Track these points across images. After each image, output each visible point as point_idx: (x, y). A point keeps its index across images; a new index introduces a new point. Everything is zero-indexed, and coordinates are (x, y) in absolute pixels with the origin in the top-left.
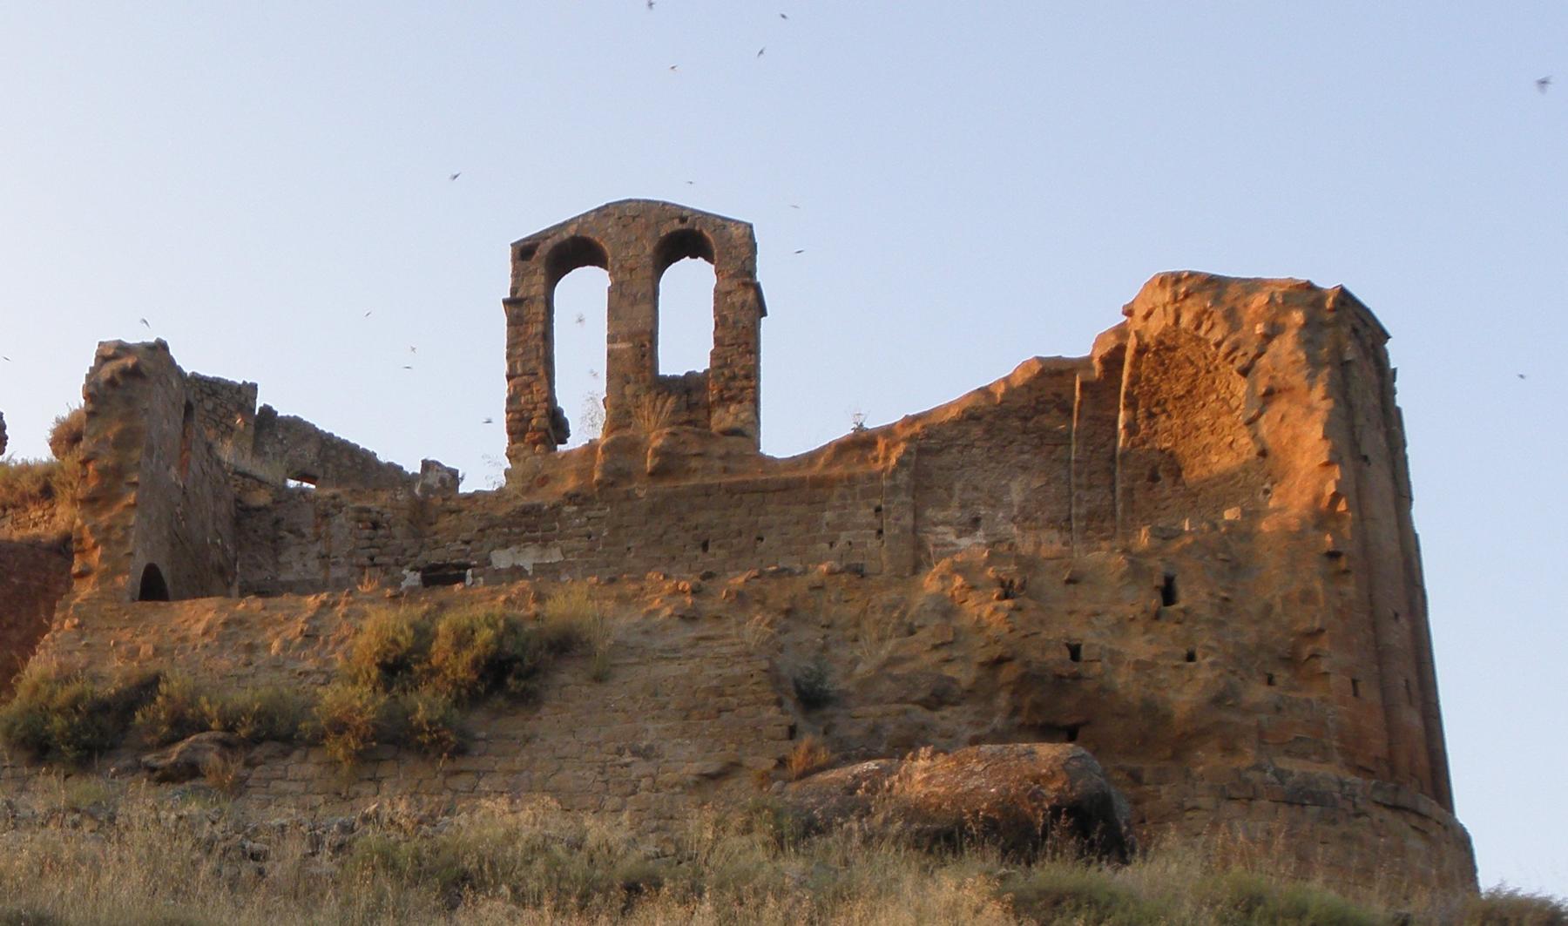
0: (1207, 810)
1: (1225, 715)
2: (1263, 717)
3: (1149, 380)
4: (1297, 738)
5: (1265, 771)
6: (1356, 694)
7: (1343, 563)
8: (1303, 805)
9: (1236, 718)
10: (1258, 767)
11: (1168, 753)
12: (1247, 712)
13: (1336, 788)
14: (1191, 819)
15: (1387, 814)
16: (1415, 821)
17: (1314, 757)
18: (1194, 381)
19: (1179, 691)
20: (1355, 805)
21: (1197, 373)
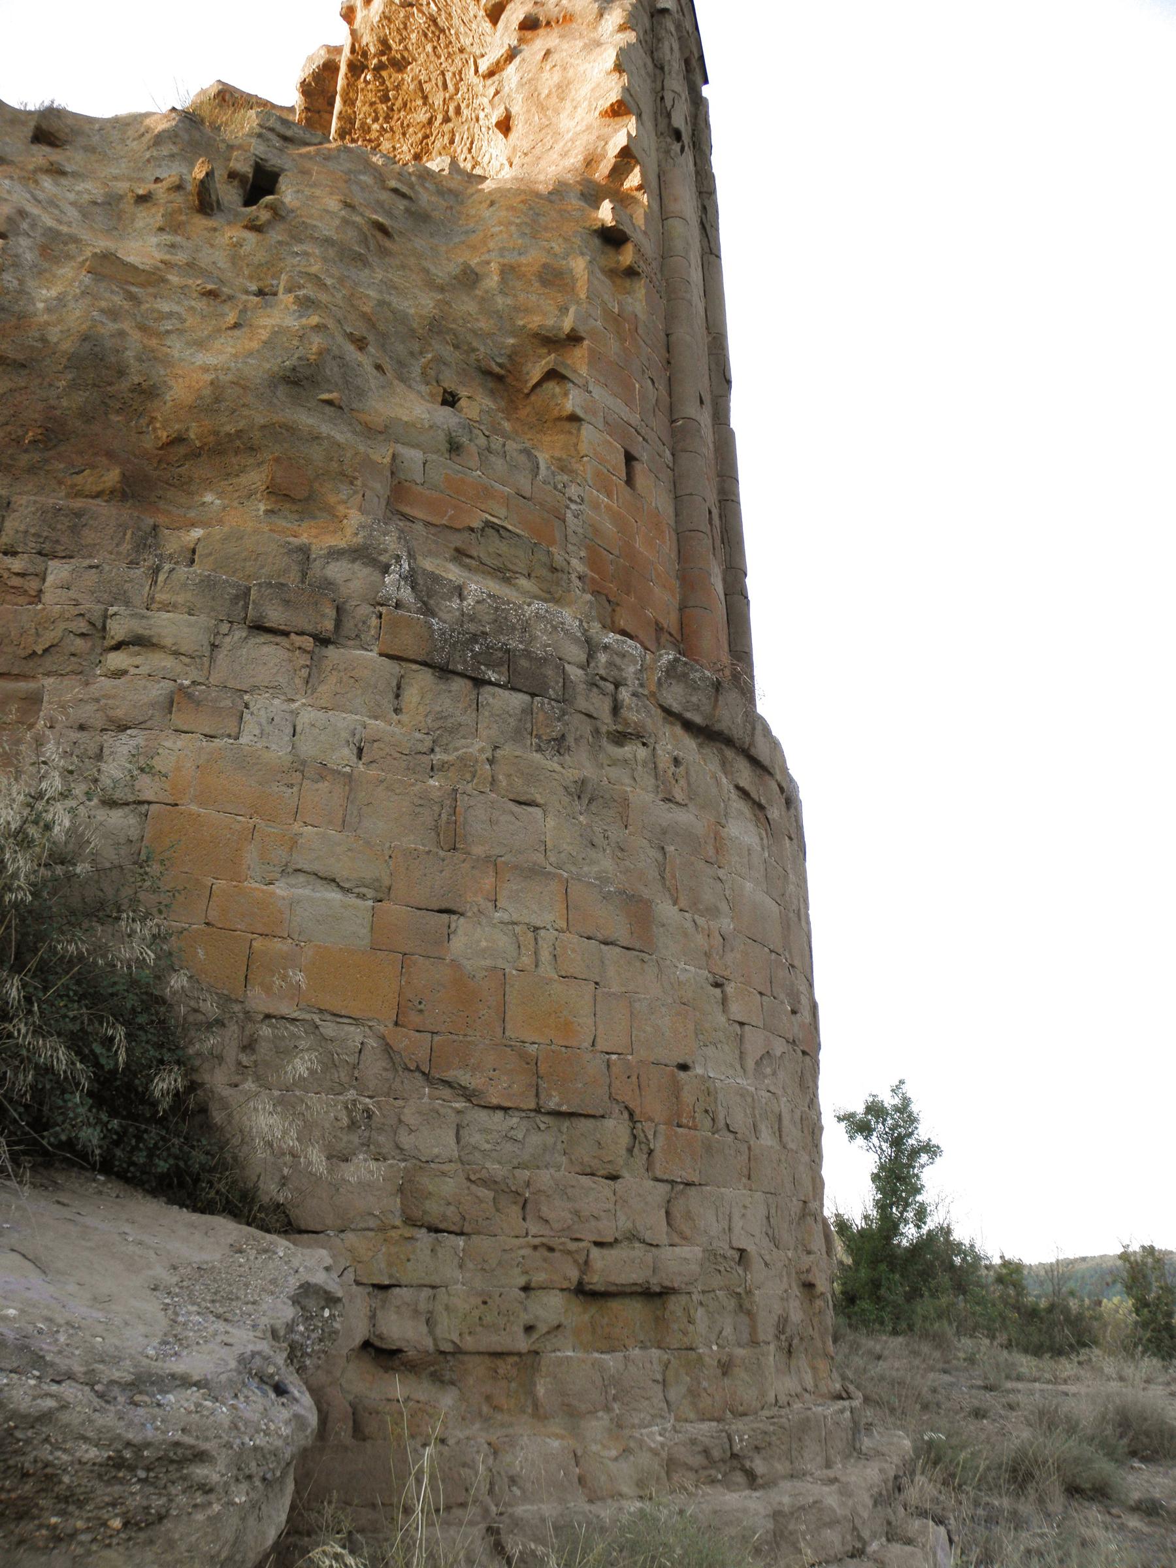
0: (177, 654)
1: (306, 419)
2: (413, 456)
3: (366, 129)
4: (488, 524)
5: (385, 569)
6: (630, 481)
7: (627, 256)
8: (479, 682)
9: (341, 434)
10: (362, 554)
11: (112, 477)
12: (371, 432)
13: (576, 653)
14: (119, 674)
15: (689, 746)
16: (745, 775)
17: (523, 582)
18: (426, 137)
19: (200, 344)
20: (616, 709)
21: (430, 122)
